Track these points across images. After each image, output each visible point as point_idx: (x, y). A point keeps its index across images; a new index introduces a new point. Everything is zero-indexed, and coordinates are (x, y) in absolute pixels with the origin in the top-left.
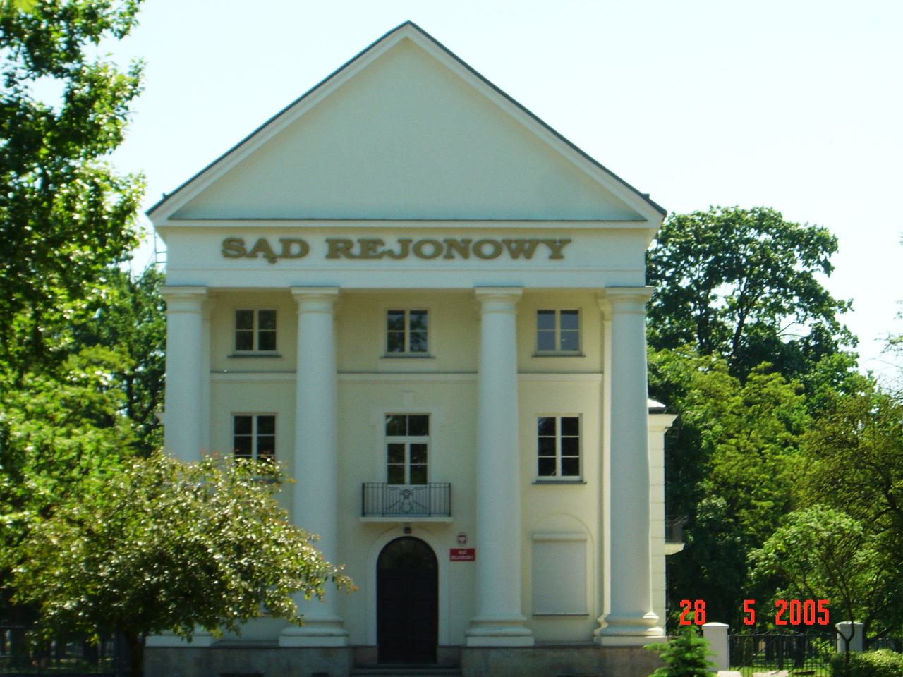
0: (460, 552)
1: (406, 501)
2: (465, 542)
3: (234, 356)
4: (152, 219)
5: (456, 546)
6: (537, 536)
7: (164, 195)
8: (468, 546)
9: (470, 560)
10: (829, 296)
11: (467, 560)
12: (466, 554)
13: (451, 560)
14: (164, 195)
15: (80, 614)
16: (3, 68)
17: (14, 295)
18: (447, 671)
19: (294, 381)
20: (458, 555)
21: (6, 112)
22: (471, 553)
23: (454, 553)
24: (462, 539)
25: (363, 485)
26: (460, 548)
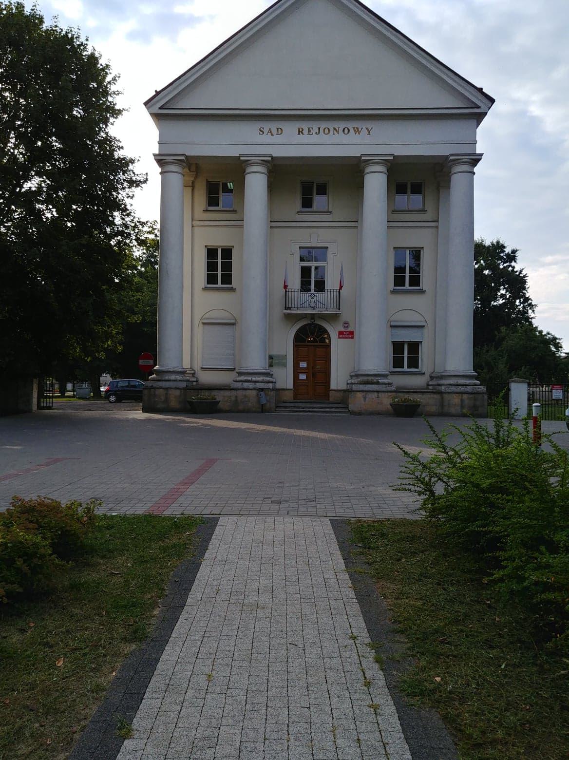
0: (344, 333)
1: (313, 300)
2: (348, 327)
3: (206, 211)
4: (148, 108)
5: (343, 330)
6: (393, 324)
7: (156, 91)
8: (349, 330)
9: (351, 338)
10: (46, 26)
11: (350, 338)
12: (348, 334)
13: (339, 338)
14: (156, 91)
15: (32, 106)
16: (2, 552)
17: (17, 123)
18: (268, 323)
19: (242, 226)
20: (343, 334)
21: (59, 393)
22: (351, 334)
23: (341, 333)
24: (346, 325)
25: (184, 186)
26: (345, 330)
